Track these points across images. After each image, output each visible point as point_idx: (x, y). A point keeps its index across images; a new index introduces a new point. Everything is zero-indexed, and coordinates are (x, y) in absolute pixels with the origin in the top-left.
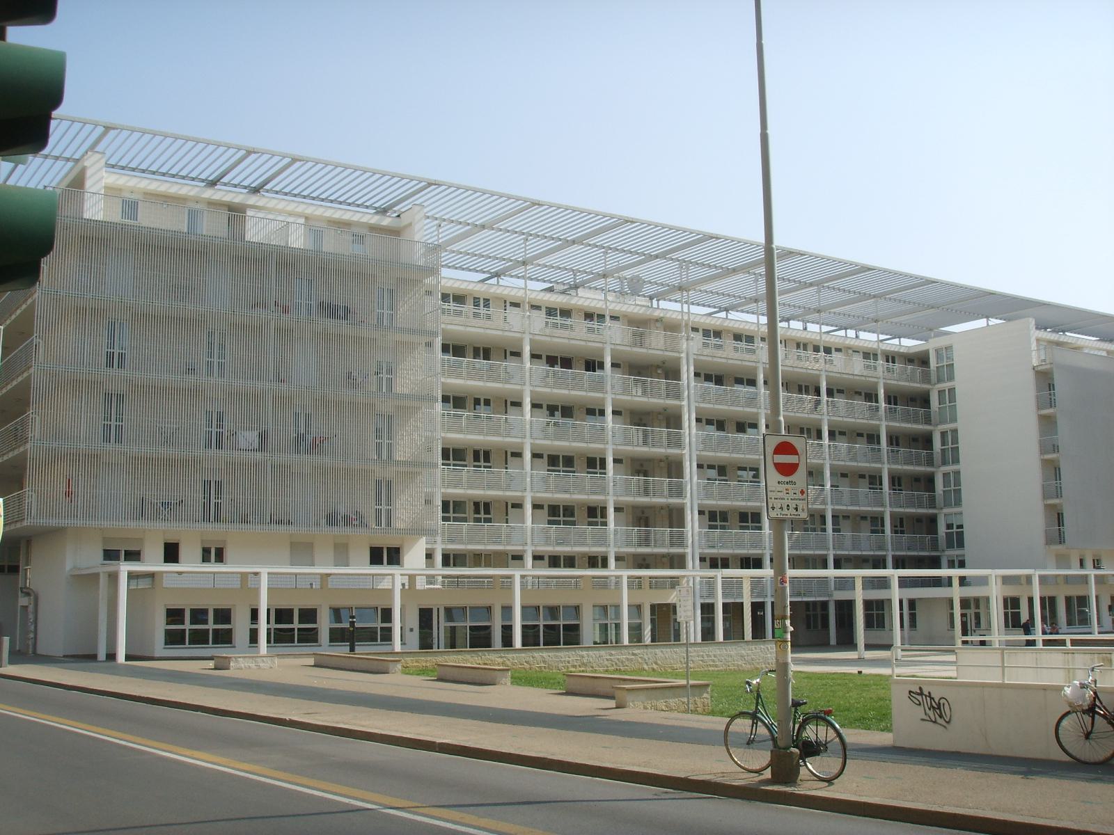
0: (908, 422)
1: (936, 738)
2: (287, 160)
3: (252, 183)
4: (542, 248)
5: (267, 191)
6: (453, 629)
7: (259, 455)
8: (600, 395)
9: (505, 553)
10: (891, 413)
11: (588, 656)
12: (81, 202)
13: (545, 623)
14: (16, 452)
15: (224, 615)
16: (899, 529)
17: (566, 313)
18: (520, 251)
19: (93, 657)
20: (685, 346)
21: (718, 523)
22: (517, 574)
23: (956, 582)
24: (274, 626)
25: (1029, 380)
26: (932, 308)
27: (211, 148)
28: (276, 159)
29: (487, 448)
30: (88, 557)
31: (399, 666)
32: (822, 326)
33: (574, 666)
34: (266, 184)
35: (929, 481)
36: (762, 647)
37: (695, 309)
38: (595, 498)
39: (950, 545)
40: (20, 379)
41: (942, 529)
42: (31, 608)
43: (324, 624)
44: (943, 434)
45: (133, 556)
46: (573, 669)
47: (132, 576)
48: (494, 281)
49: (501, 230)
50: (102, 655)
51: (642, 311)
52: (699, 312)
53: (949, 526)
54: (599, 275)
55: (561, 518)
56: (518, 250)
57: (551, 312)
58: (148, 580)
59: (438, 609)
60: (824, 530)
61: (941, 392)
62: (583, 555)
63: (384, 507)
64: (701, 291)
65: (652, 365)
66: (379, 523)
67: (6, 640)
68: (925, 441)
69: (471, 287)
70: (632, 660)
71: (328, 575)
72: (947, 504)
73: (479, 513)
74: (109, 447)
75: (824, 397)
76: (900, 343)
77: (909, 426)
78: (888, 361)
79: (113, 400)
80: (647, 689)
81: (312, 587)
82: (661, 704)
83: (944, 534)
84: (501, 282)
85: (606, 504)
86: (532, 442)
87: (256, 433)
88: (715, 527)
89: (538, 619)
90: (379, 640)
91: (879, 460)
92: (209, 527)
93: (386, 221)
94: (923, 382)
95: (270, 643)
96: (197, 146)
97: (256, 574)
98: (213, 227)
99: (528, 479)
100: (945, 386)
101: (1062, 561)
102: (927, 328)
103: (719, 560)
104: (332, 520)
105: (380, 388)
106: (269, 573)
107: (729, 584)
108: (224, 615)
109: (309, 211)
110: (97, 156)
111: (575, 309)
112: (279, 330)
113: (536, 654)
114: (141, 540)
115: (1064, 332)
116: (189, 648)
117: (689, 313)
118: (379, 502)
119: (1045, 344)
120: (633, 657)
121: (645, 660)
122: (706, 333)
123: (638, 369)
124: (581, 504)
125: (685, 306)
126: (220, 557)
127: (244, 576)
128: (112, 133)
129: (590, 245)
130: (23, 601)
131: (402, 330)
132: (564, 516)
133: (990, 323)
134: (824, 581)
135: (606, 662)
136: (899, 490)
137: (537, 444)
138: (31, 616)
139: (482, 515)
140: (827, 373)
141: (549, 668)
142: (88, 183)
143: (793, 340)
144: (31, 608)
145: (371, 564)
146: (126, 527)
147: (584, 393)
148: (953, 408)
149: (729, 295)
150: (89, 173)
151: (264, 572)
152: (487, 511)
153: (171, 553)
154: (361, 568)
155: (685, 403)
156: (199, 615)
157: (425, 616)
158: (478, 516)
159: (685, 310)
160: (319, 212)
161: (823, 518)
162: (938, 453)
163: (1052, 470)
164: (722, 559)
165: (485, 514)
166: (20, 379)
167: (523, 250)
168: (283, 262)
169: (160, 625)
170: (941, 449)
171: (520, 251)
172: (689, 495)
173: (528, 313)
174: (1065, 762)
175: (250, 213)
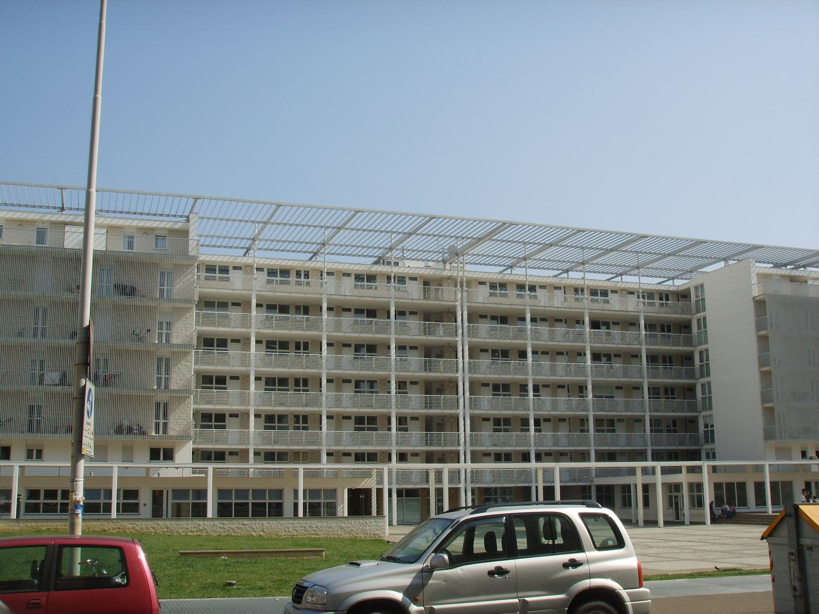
0: (653, 344)
4: (592, 254)
6: (179, 505)
7: (59, 388)
8: (245, 330)
10: (650, 339)
11: (204, 525)
13: (193, 502)
16: (672, 428)
18: (522, 253)
21: (502, 427)
22: (386, 467)
23: (639, 472)
24: (122, 501)
27: (334, 211)
28: (346, 212)
35: (691, 389)
36: (361, 521)
39: (707, 442)
41: (701, 428)
46: (191, 534)
53: (706, 426)
54: (634, 267)
56: (579, 255)
59: (167, 490)
60: (389, 429)
63: (161, 421)
64: (648, 268)
66: (157, 432)
70: (241, 528)
72: (704, 409)
73: (299, 423)
75: (529, 325)
76: (673, 283)
83: (703, 432)
85: (390, 414)
86: (533, 377)
88: (499, 430)
90: (121, 512)
92: (30, 436)
95: (119, 512)
96: (312, 210)
101: (782, 452)
104: (119, 430)
106: (118, 467)
111: (379, 274)
113: (160, 523)
116: (122, 515)
120: (243, 526)
121: (253, 528)
122: (493, 286)
128: (281, 208)
129: (563, 246)
134: (588, 470)
135: (219, 530)
136: (672, 398)
139: (301, 425)
140: (589, 311)
141: (170, 532)
143: (476, 280)
145: (355, 461)
147: (371, 335)
148: (706, 332)
149: (666, 269)
154: (142, 463)
155: (459, 339)
156: (51, 494)
158: (298, 425)
161: (389, 419)
162: (698, 368)
164: (505, 454)
165: (303, 423)
167: (524, 252)
171: (522, 253)
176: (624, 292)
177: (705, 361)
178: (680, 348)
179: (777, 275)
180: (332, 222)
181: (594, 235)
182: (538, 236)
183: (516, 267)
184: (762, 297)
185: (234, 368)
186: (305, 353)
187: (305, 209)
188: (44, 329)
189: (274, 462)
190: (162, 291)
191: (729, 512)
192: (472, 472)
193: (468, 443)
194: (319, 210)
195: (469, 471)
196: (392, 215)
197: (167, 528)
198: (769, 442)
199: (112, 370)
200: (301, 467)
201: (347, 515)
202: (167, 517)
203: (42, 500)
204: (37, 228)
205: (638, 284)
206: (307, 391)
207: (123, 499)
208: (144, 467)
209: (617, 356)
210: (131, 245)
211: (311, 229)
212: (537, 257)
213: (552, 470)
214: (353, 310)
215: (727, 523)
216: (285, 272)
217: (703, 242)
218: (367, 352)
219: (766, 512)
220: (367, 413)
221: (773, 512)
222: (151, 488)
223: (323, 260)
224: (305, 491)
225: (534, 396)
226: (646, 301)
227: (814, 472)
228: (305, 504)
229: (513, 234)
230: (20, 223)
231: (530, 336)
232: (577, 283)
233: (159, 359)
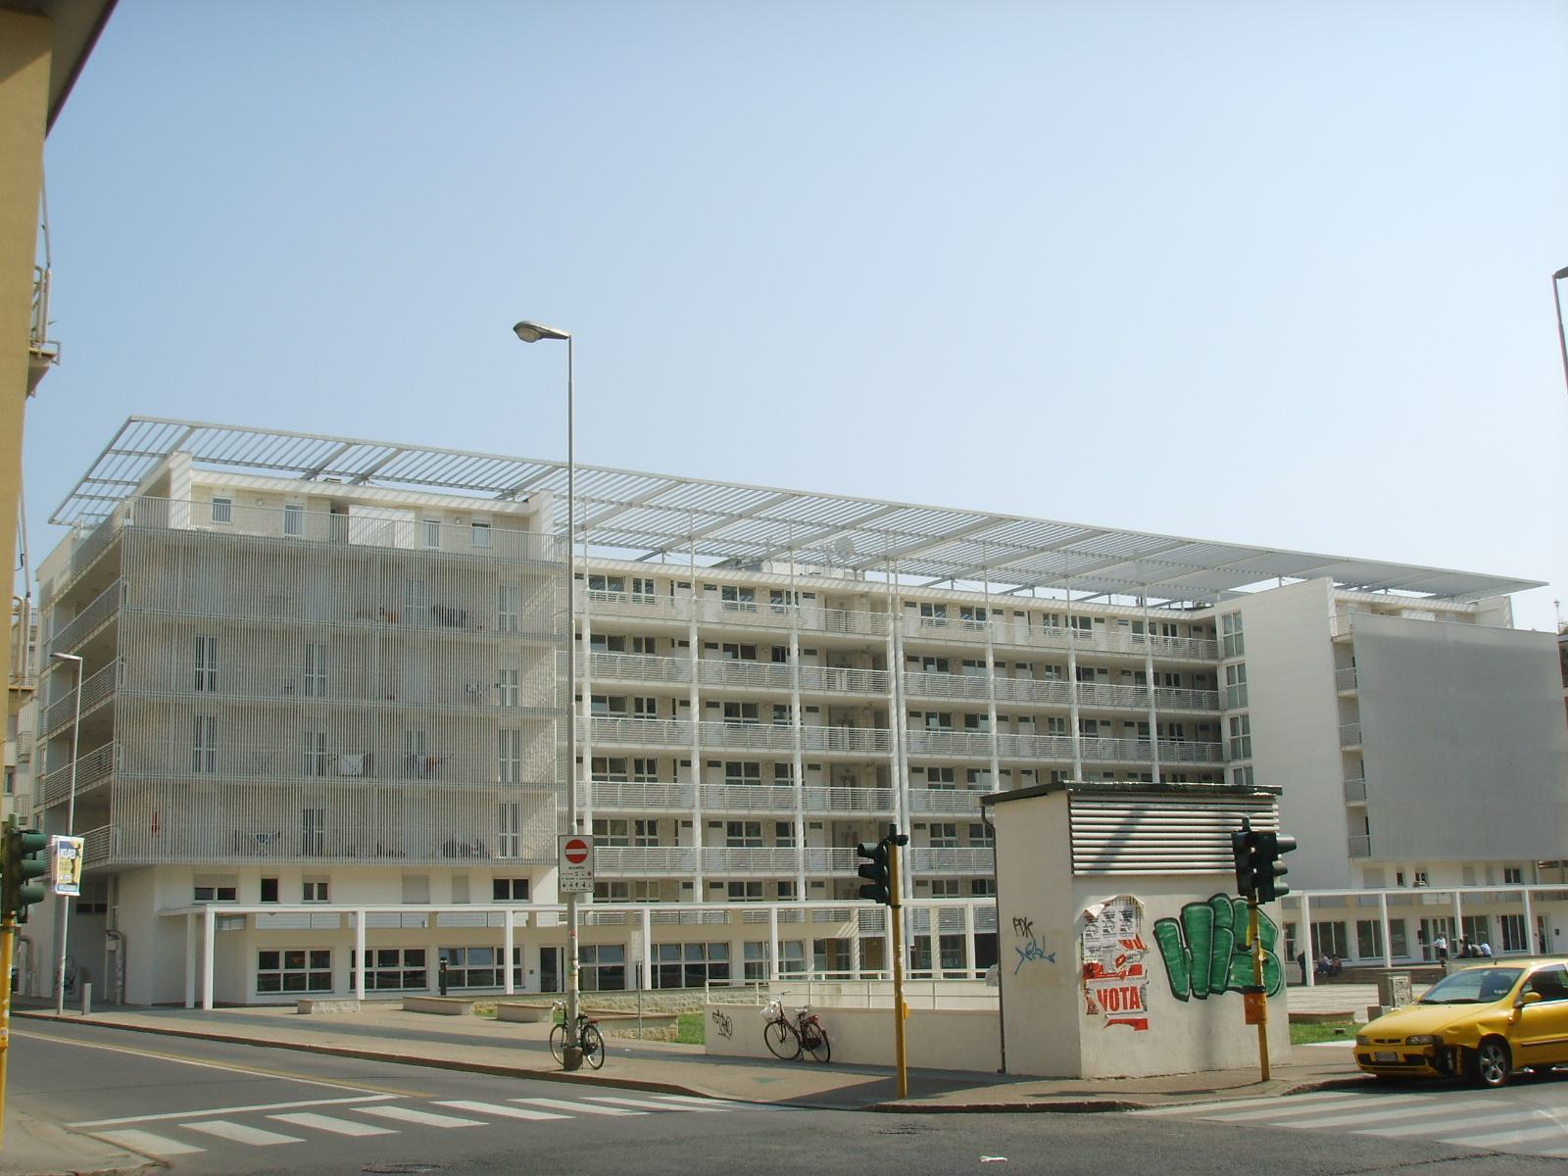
0: (1184, 707)
1: (726, 1047)
2: (392, 450)
3: (359, 470)
5: (377, 478)
7: (364, 782)
8: (784, 691)
9: (675, 881)
12: (167, 509)
14: (100, 783)
15: (322, 958)
17: (748, 592)
19: (182, 1005)
20: (891, 627)
25: (1327, 653)
26: (1205, 569)
29: (651, 758)
30: (175, 896)
31: (472, 1008)
32: (1071, 591)
33: (691, 1009)
34: (376, 471)
37: (904, 579)
38: (781, 814)
40: (103, 703)
42: (119, 953)
43: (432, 967)
44: (1233, 721)
45: (227, 894)
46: (689, 1013)
47: (220, 918)
48: (658, 558)
49: (651, 507)
50: (190, 1003)
51: (841, 586)
52: (911, 583)
55: (744, 838)
57: (729, 592)
58: (241, 921)
61: (1230, 669)
62: (771, 881)
65: (856, 651)
67: (88, 987)
68: (1210, 730)
69: (628, 568)
71: (436, 913)
73: (643, 834)
74: (202, 776)
76: (1110, 601)
77: (1187, 712)
78: (1166, 634)
79: (204, 727)
80: (615, 1019)
81: (423, 927)
82: (629, 1032)
84: (668, 560)
87: (361, 756)
89: (679, 959)
91: (1150, 757)
93: (511, 507)
94: (1210, 658)
97: (354, 913)
98: (313, 529)
99: (697, 794)
100: (1233, 661)
102: (1211, 590)
103: (945, 883)
104: (449, 850)
105: (503, 702)
106: (366, 912)
107: (946, 914)
108: (322, 958)
109: (422, 501)
110: (183, 456)
112: (385, 640)
114: (235, 877)
115: (1386, 588)
117: (897, 585)
118: (504, 828)
119: (1355, 606)
122: (926, 609)
123: (839, 657)
124: (768, 820)
125: (892, 575)
126: (324, 895)
127: (344, 915)
128: (198, 432)
130: (111, 945)
131: (525, 635)
132: (747, 835)
133: (1284, 583)
137: (914, 701)
138: (119, 962)
142: (174, 487)
143: (1040, 611)
144: (119, 953)
146: (217, 864)
148: (1243, 689)
150: (174, 475)
151: (362, 911)
152: (652, 831)
153: (270, 891)
154: (482, 903)
156: (295, 958)
157: (548, 957)
158: (642, 837)
159: (892, 581)
160: (434, 501)
163: (1354, 763)
166: (103, 703)
168: (390, 564)
169: (252, 970)
170: (1232, 740)
172: (898, 806)
173: (695, 598)
174: (773, 1059)
175: (353, 510)
176: (1115, 621)
177: (1241, 733)
178: (1203, 713)
179: (1354, 602)
180: (161, 444)
181: (626, 481)
182: (504, 476)
183: (672, 551)
184: (1348, 637)
185: (1024, 759)
186: (748, 722)
187: (166, 427)
188: (212, 676)
189: (606, 899)
190: (501, 619)
191: (1331, 966)
192: (915, 911)
193: (908, 865)
194: (156, 427)
195: (910, 909)
196: (226, 432)
197: (656, 1005)
198: (1358, 860)
199: (432, 750)
200: (647, 909)
201: (650, 988)
202: (563, 990)
203: (282, 970)
204: (288, 507)
205: (886, 587)
206: (655, 780)
207: (286, 968)
208: (426, 912)
209: (1105, 723)
210: (433, 539)
211: (133, 458)
212: (606, 524)
213: (961, 912)
214: (721, 647)
215: (1330, 983)
216: (616, 581)
217: (795, 495)
218: (611, 710)
219: (1383, 966)
220: (744, 817)
221: (1393, 966)
222: (258, 948)
223: (583, 555)
224: (780, 944)
225: (594, 778)
226: (1079, 630)
227: (1429, 906)
228: (654, 969)
229: (498, 475)
230: (260, 496)
231: (994, 691)
232: (911, 593)
233: (503, 734)
